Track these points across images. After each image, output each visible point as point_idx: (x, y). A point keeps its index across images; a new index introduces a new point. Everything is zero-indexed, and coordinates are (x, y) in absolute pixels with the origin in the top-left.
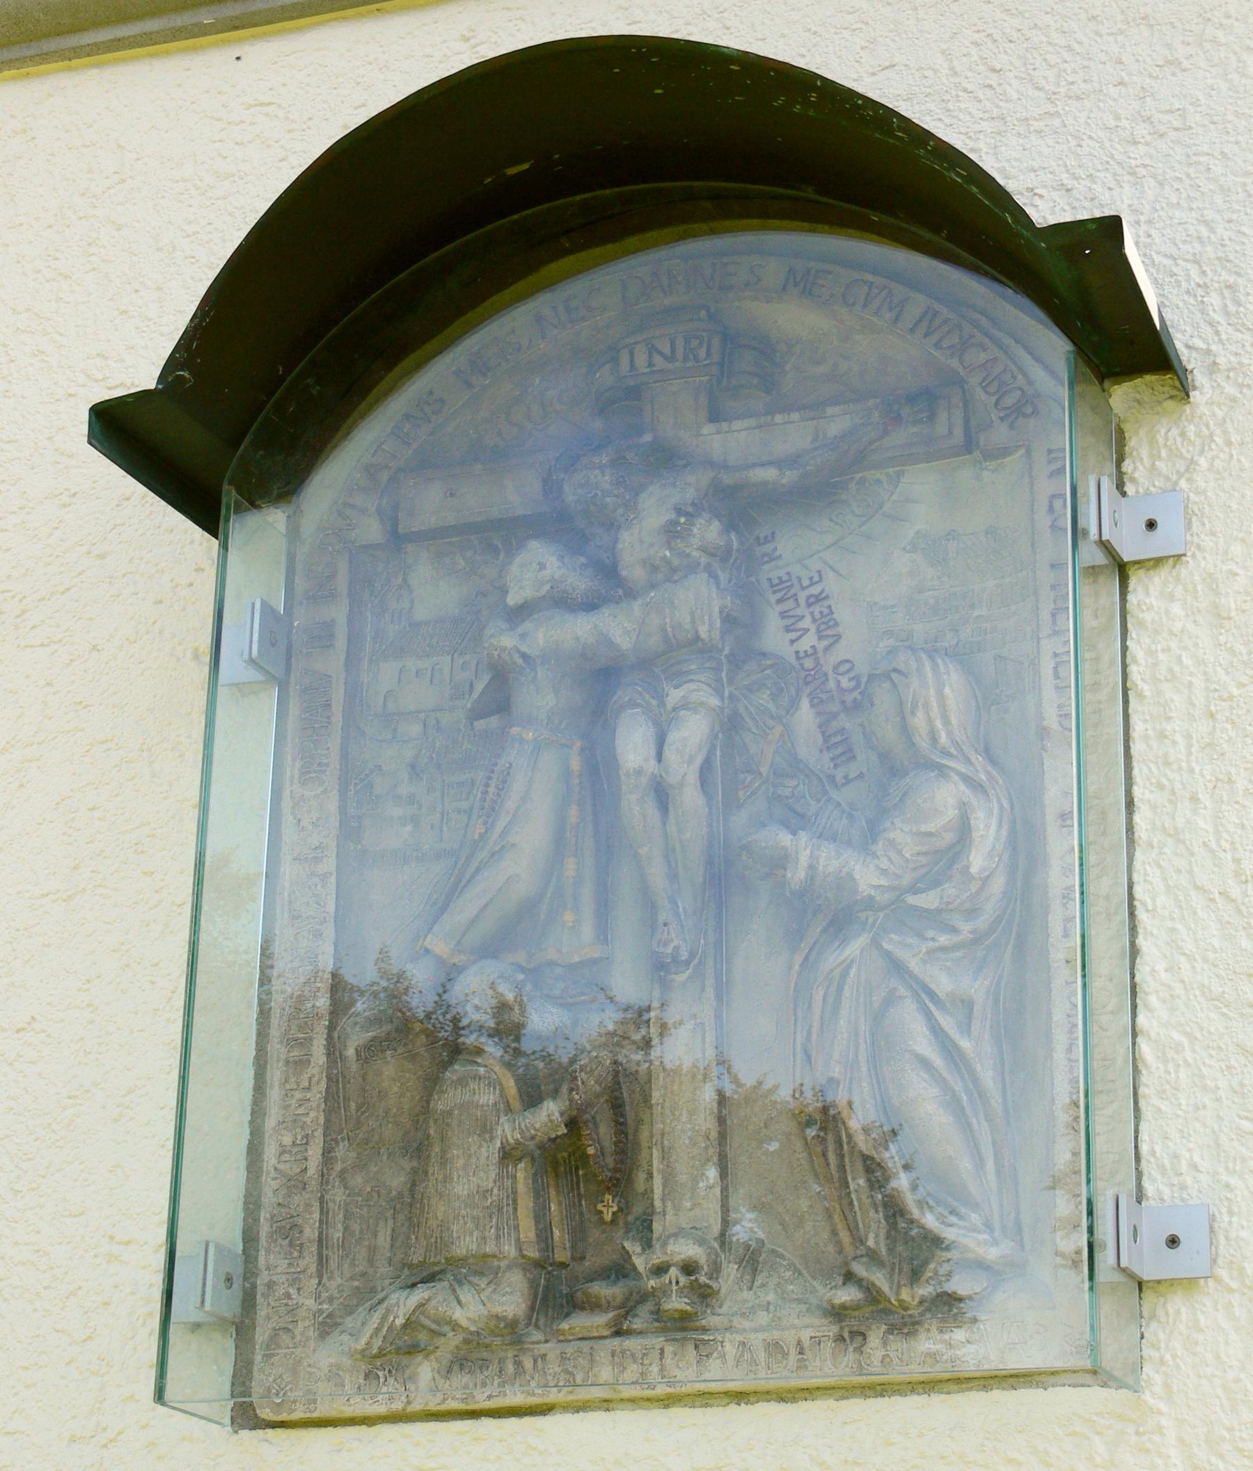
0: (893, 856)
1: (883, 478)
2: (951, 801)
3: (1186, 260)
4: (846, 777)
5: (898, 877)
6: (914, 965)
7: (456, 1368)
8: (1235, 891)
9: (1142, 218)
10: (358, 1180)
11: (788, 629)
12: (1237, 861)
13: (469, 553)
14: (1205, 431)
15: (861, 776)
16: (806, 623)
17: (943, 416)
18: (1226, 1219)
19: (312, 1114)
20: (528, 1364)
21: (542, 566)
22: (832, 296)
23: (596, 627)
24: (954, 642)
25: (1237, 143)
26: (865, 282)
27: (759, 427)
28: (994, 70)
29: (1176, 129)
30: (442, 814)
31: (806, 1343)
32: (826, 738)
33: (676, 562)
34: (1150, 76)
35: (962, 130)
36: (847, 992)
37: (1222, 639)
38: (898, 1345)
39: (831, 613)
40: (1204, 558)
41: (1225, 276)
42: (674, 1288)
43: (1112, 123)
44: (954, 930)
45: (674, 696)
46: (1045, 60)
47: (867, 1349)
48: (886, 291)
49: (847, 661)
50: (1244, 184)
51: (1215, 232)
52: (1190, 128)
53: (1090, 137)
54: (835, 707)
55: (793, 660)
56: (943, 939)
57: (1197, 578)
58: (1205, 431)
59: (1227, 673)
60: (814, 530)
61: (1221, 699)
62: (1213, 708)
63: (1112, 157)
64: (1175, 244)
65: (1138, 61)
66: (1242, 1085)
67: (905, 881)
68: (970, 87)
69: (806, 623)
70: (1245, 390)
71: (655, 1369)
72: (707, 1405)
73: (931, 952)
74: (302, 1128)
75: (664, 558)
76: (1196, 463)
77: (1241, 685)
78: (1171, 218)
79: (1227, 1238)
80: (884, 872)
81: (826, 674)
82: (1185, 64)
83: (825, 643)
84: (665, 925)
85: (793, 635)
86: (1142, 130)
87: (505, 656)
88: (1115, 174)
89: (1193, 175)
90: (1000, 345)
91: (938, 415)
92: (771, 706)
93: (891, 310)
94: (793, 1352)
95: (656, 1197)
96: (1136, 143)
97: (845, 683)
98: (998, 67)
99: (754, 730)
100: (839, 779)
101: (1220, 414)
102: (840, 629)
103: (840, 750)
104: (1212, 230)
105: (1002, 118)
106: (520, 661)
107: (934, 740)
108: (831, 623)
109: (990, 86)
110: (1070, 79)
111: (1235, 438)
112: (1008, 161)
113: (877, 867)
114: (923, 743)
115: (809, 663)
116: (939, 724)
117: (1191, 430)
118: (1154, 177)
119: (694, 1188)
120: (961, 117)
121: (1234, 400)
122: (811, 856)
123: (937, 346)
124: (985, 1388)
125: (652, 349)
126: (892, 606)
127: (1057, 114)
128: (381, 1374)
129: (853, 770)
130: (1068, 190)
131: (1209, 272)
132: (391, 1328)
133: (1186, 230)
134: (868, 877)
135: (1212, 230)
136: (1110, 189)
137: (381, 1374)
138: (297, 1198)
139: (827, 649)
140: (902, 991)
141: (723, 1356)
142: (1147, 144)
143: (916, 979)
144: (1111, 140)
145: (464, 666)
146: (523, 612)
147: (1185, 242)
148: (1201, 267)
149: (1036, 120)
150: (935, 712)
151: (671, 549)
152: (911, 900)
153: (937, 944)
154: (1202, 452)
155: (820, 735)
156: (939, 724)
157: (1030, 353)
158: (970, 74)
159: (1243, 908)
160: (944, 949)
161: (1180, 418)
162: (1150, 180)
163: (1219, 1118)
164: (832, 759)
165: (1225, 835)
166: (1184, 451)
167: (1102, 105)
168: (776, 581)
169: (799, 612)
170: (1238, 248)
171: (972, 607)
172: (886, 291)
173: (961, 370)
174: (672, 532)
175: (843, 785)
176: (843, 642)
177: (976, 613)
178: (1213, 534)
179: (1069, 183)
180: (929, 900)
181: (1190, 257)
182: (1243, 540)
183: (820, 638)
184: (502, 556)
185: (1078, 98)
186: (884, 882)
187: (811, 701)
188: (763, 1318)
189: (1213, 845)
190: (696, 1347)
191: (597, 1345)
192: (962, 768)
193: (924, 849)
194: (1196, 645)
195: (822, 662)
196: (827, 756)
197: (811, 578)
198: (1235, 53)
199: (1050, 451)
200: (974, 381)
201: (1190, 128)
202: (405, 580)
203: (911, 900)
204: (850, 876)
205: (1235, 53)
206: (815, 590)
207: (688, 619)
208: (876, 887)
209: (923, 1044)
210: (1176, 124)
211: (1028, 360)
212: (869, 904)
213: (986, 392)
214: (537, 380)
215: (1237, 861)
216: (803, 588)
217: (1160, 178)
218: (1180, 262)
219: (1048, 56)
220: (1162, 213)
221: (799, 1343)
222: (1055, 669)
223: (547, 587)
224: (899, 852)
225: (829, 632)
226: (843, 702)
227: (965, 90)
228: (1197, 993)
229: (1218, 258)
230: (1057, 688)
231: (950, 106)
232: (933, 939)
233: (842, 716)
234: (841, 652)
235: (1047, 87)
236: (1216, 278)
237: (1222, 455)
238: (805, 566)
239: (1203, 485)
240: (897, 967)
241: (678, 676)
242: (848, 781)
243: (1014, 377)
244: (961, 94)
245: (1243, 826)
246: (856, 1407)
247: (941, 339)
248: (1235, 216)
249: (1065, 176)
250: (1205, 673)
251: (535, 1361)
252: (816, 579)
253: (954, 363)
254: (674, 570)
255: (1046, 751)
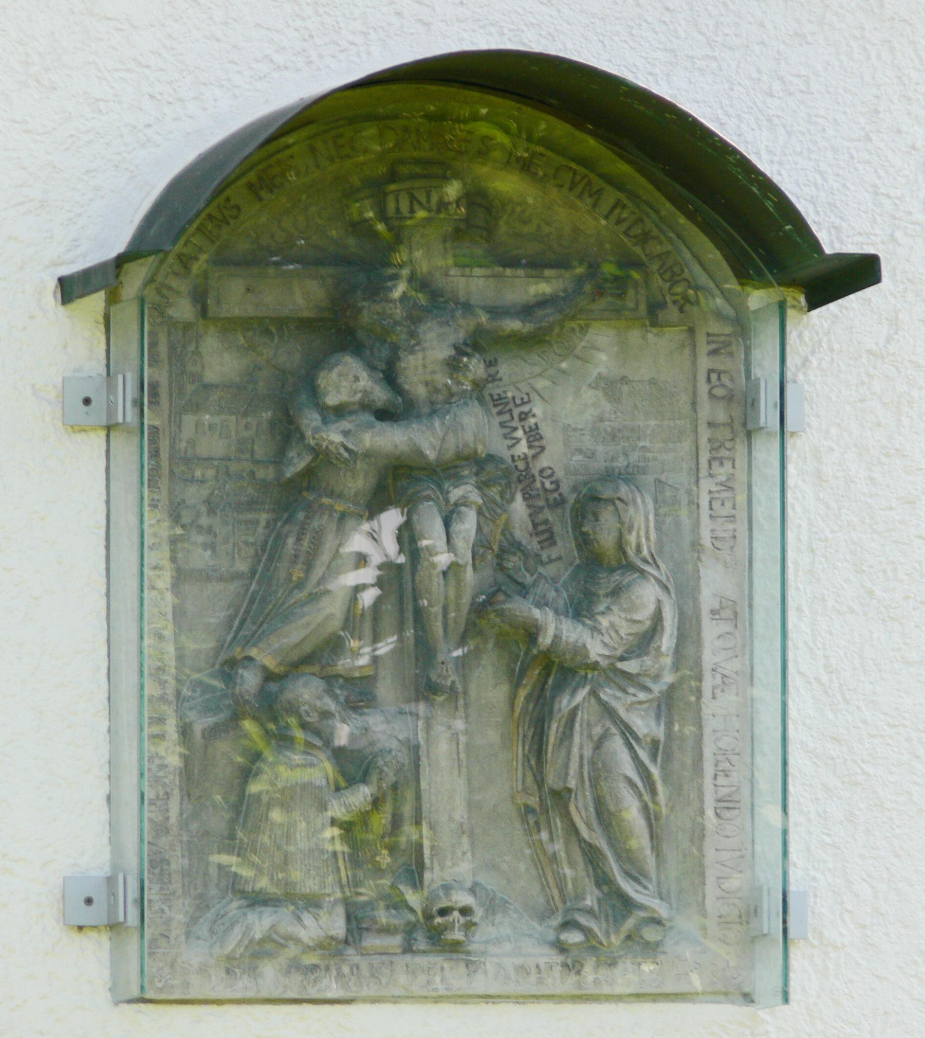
0: (613, 634)
1: (576, 326)
2: (652, 599)
3: (806, 200)
4: (549, 557)
5: (615, 649)
6: (622, 712)
7: (293, 970)
8: (825, 678)
9: (776, 159)
10: (194, 826)
11: (505, 437)
12: (827, 657)
13: (250, 334)
14: (816, 338)
15: (560, 558)
16: (520, 433)
17: (631, 292)
18: (812, 900)
19: (171, 777)
20: (346, 970)
21: (357, 379)
22: (545, 175)
23: (411, 439)
24: (625, 463)
25: (845, 113)
26: (570, 168)
27: (494, 276)
28: (668, 9)
29: (801, 91)
30: (234, 545)
31: (542, 966)
32: (535, 526)
33: (455, 389)
34: (784, 42)
35: (644, 54)
36: (577, 726)
37: (821, 495)
38: (604, 972)
39: (537, 428)
40: (812, 434)
41: (833, 219)
42: (457, 925)
43: (755, 75)
44: (647, 689)
45: (456, 494)
46: (706, 9)
47: (583, 973)
48: (586, 180)
49: (550, 468)
50: (849, 148)
51: (826, 181)
52: (813, 93)
53: (740, 84)
54: (541, 503)
55: (509, 460)
56: (642, 696)
57: (807, 449)
58: (816, 338)
59: (824, 521)
60: (525, 361)
61: (820, 540)
62: (814, 546)
63: (755, 103)
64: (798, 185)
65: (775, 28)
66: (825, 812)
67: (619, 653)
68: (650, 19)
69: (520, 433)
70: (844, 311)
71: (438, 979)
72: (465, 1003)
73: (632, 704)
74: (163, 787)
75: (446, 385)
76: (811, 362)
77: (833, 532)
78: (796, 163)
79: (813, 913)
80: (606, 644)
81: (533, 476)
82: (810, 39)
83: (533, 452)
84: (443, 663)
85: (510, 442)
86: (777, 86)
87: (331, 448)
88: (757, 119)
89: (813, 132)
90: (670, 240)
91: (621, 286)
92: (498, 498)
93: (591, 196)
94: (533, 970)
95: (425, 856)
96: (772, 96)
97: (548, 485)
98: (672, 8)
99: (487, 515)
100: (544, 557)
101: (826, 325)
102: (544, 442)
103: (546, 536)
104: (825, 179)
105: (672, 51)
106: (346, 455)
107: (639, 549)
108: (538, 437)
109: (665, 22)
110: (725, 31)
111: (836, 346)
112: (678, 89)
113: (602, 641)
114: (631, 552)
115: (521, 465)
116: (644, 541)
117: (806, 334)
118: (784, 126)
119: (453, 853)
120: (642, 43)
121: (836, 316)
122: (556, 628)
123: (626, 233)
124: (654, 1001)
125: (413, 198)
126: (581, 430)
127: (715, 59)
128: (237, 970)
129: (554, 552)
130: (721, 124)
131: (822, 213)
132: (251, 941)
133: (806, 175)
134: (596, 650)
135: (825, 179)
136: (753, 129)
137: (237, 970)
138: (163, 839)
139: (535, 457)
140: (614, 730)
141: (485, 972)
142: (779, 98)
143: (622, 721)
144: (754, 89)
145: (247, 427)
146: (340, 411)
147: (805, 185)
148: (816, 207)
149: (699, 59)
150: (642, 533)
151: (451, 378)
152: (620, 665)
153: (637, 699)
154: (813, 352)
155: (530, 523)
156: (644, 541)
157: (688, 248)
158: (649, 8)
159: (830, 691)
160: (640, 703)
161: (799, 323)
162: (782, 128)
163: (810, 832)
164: (539, 542)
165: (819, 638)
166: (800, 350)
167: (748, 58)
168: (496, 397)
169: (514, 424)
170: (843, 199)
171: (639, 439)
172: (586, 180)
173: (643, 256)
174: (453, 366)
175: (547, 563)
176: (546, 452)
177: (641, 444)
178: (818, 416)
179: (724, 119)
180: (631, 666)
181: (809, 198)
182: (839, 425)
183: (530, 447)
184: (276, 340)
185: (731, 48)
186: (607, 653)
187: (524, 495)
188: (508, 947)
189: (811, 644)
190: (467, 966)
191: (394, 959)
192: (656, 573)
193: (633, 631)
194: (804, 498)
195: (531, 465)
196: (535, 540)
197: (522, 399)
198: (846, 38)
199: (708, 335)
200: (655, 267)
201: (813, 93)
202: (197, 347)
203: (620, 665)
204: (584, 646)
205: (846, 38)
206: (525, 408)
207: (472, 438)
208: (600, 655)
209: (629, 769)
210: (802, 87)
211: (683, 248)
212: (595, 666)
213: (662, 278)
214: (304, 197)
215: (827, 657)
216: (516, 406)
217: (789, 128)
218: (801, 200)
219: (709, 8)
220: (790, 158)
221: (537, 966)
222: (710, 502)
223: (359, 395)
224: (617, 631)
225: (537, 444)
226: (547, 500)
227: (646, 21)
228: (799, 746)
229: (829, 203)
230: (711, 516)
231: (634, 32)
232: (634, 695)
233: (546, 511)
234: (544, 461)
235: (708, 34)
236: (827, 219)
237: (827, 358)
238: (517, 388)
239: (813, 379)
240: (609, 712)
241: (458, 480)
242: (551, 561)
243: (683, 271)
244: (643, 23)
245: (831, 633)
246: (568, 1009)
247: (629, 228)
248: (841, 172)
249: (720, 111)
250: (809, 519)
251: (352, 969)
252: (526, 399)
253: (638, 250)
254: (452, 395)
255: (701, 561)
